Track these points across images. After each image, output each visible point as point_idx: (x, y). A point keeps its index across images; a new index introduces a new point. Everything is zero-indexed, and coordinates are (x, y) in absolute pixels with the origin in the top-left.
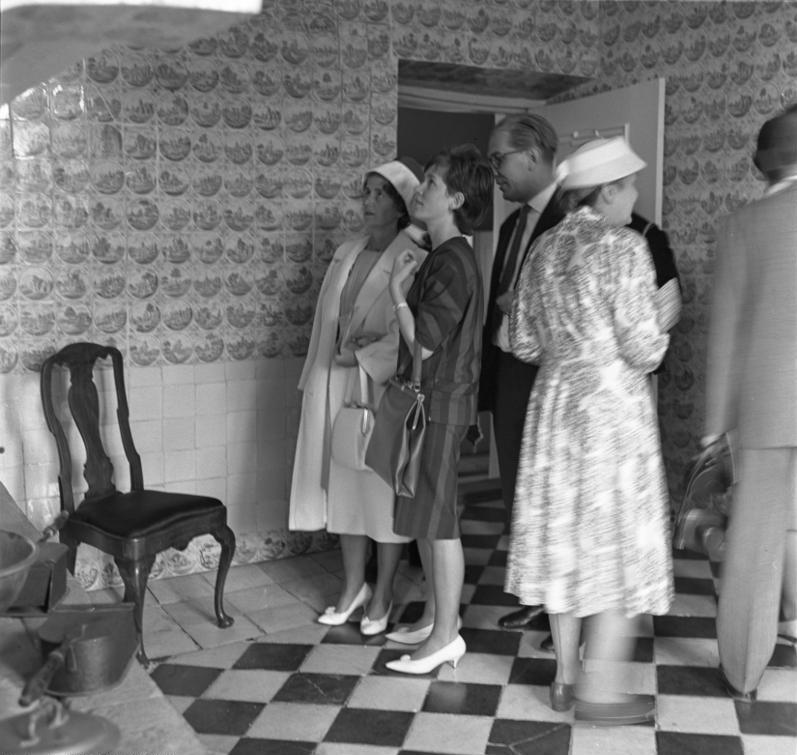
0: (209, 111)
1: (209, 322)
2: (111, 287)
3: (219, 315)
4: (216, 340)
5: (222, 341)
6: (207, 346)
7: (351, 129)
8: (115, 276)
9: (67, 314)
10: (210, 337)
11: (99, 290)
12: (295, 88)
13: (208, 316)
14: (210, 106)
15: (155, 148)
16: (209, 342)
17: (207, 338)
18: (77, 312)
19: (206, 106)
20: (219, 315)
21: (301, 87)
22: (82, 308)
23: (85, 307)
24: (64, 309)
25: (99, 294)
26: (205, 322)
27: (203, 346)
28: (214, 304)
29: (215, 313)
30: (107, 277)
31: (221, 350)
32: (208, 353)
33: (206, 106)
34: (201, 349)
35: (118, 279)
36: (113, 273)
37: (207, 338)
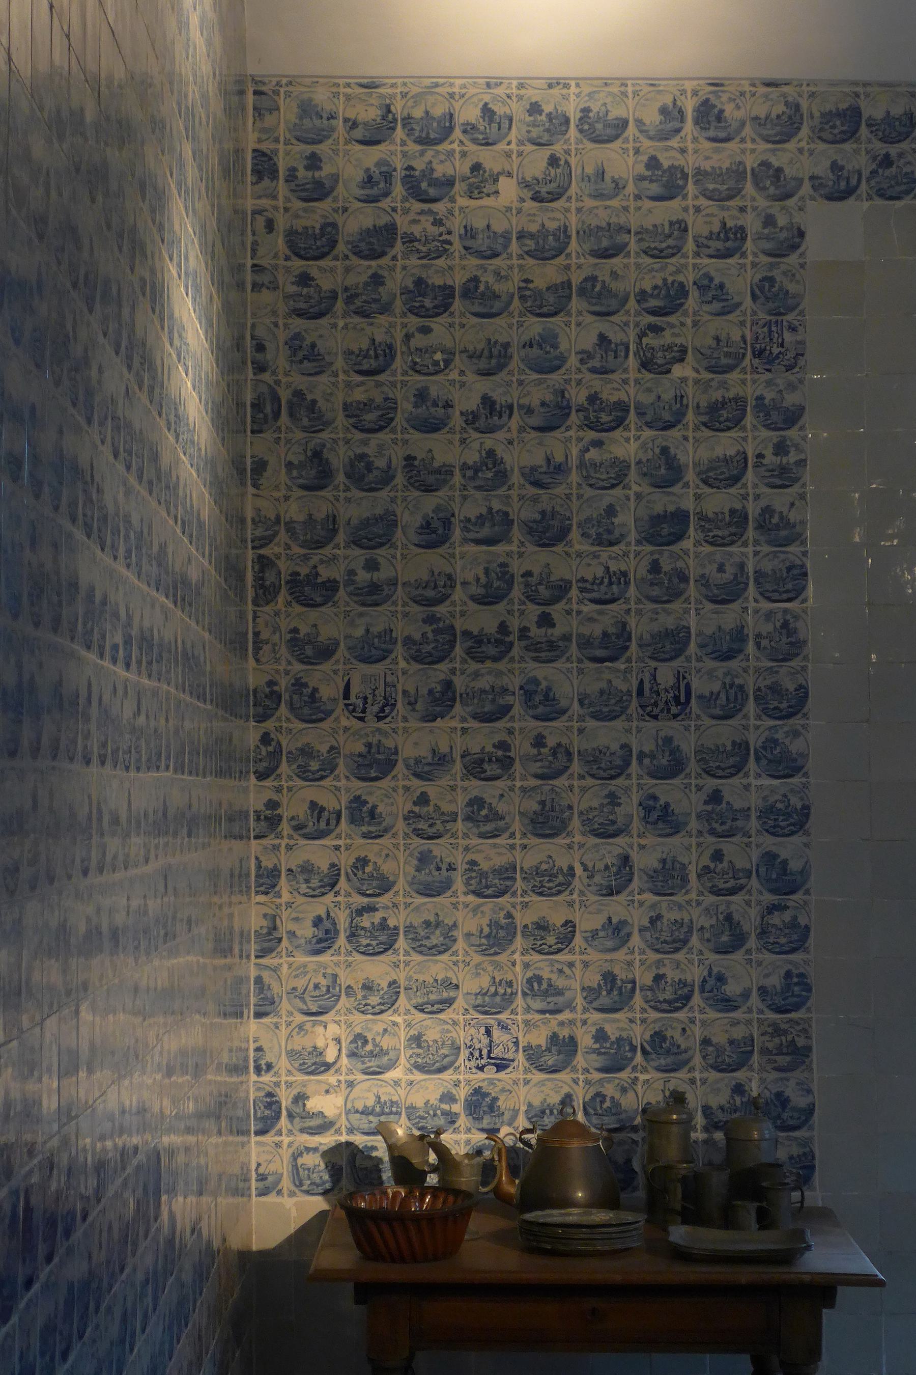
0: (728, 576)
1: (371, 477)
2: (724, 412)
3: (389, 467)
4: (441, 625)
5: (452, 627)
6: (424, 635)
7: (477, 309)
8: (731, 394)
9: (648, 166)
10: (431, 619)
11: (704, 418)
12: (424, 185)
13: (369, 467)
14: (728, 568)
15: (627, 356)
16: (428, 629)
17: (425, 621)
18: (666, 164)
19: (721, 569)
20: (389, 467)
21: (434, 183)
22: (673, 158)
23: (679, 156)
24: (645, 158)
25: (705, 424)
26: (362, 477)
27: (417, 636)
28: (381, 447)
29: (381, 463)
30: (717, 395)
31: (452, 643)
32: (428, 648)
33: (721, 569)
34: (414, 643)
35: (736, 399)
36: (728, 389)
37: (425, 621)
